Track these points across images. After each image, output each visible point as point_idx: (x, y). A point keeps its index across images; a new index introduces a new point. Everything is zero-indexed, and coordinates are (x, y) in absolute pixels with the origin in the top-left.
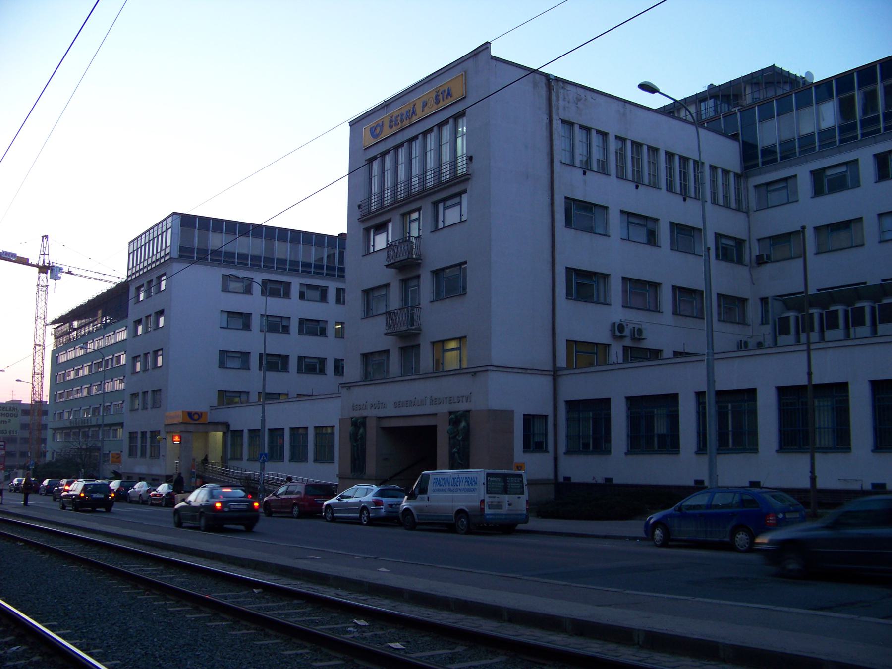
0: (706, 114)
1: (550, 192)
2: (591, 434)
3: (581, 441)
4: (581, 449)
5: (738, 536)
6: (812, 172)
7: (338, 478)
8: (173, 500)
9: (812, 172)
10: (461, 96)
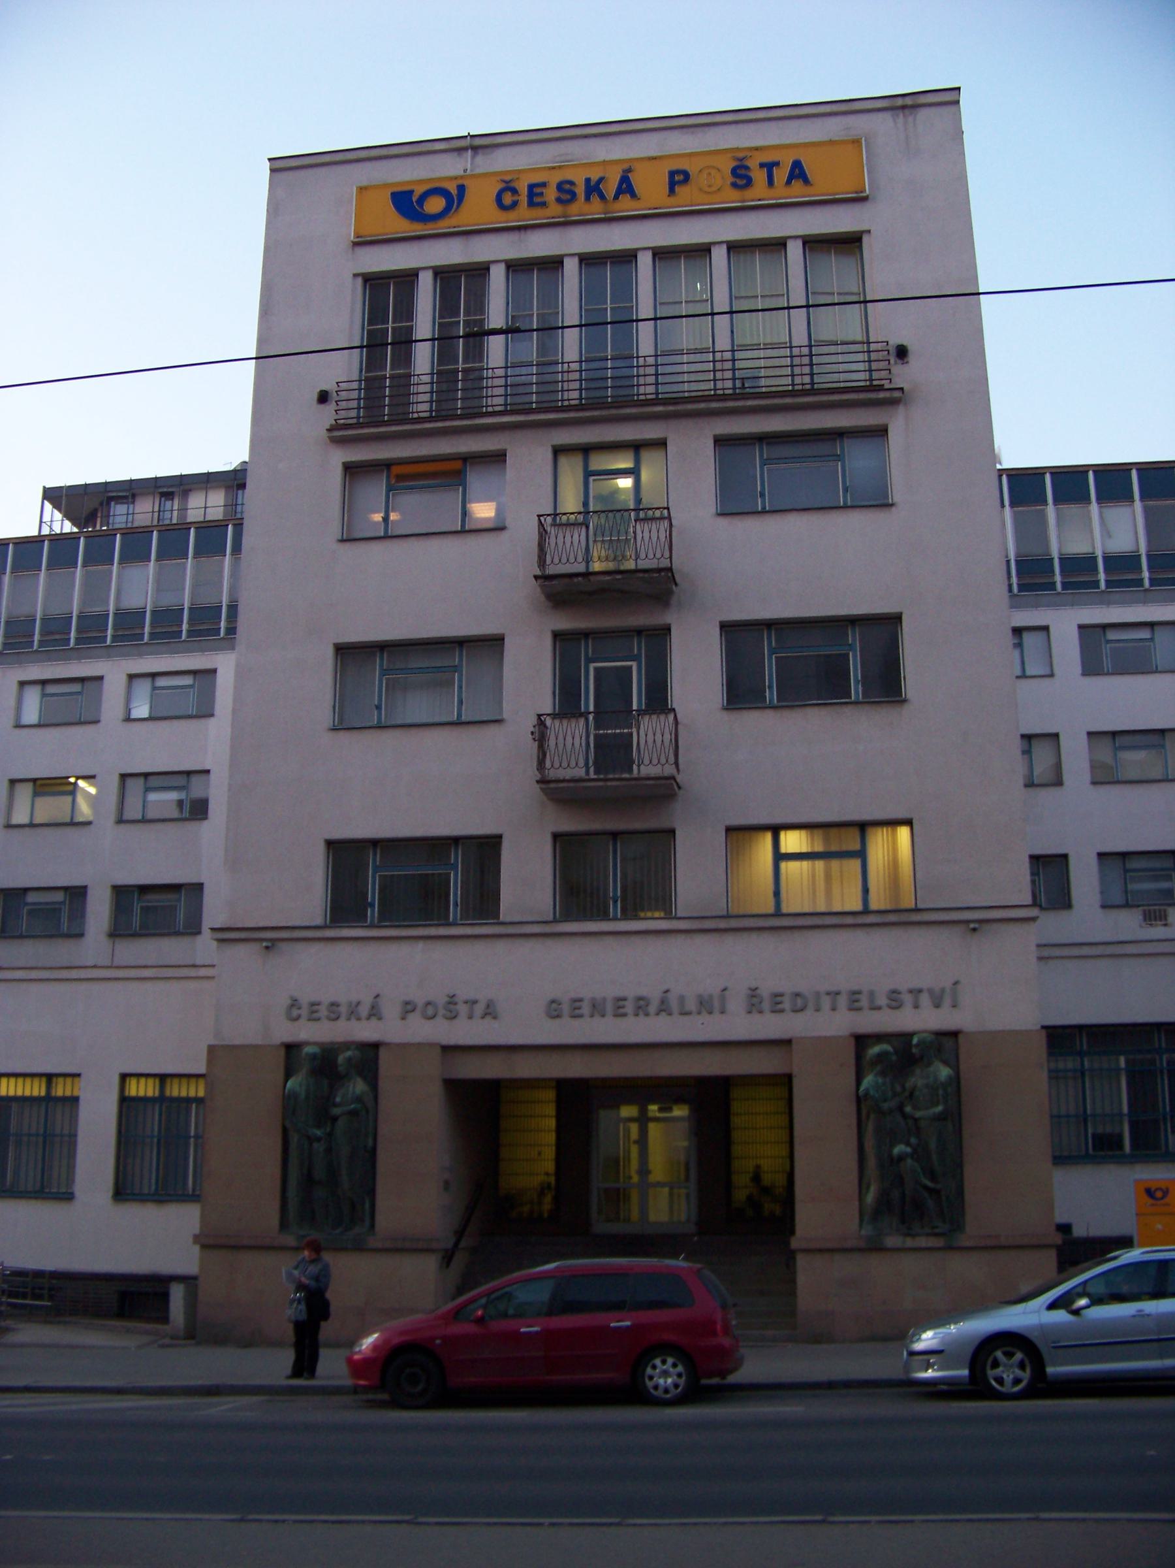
0: (236, 505)
1: (483, 533)
2: (1125, 1110)
3: (1090, 1131)
4: (1091, 1151)
5: (670, 1361)
6: (1081, 627)
7: (197, 1248)
8: (305, 1374)
9: (1081, 627)
10: (856, 193)
